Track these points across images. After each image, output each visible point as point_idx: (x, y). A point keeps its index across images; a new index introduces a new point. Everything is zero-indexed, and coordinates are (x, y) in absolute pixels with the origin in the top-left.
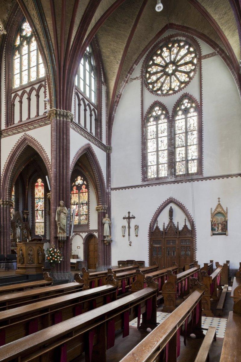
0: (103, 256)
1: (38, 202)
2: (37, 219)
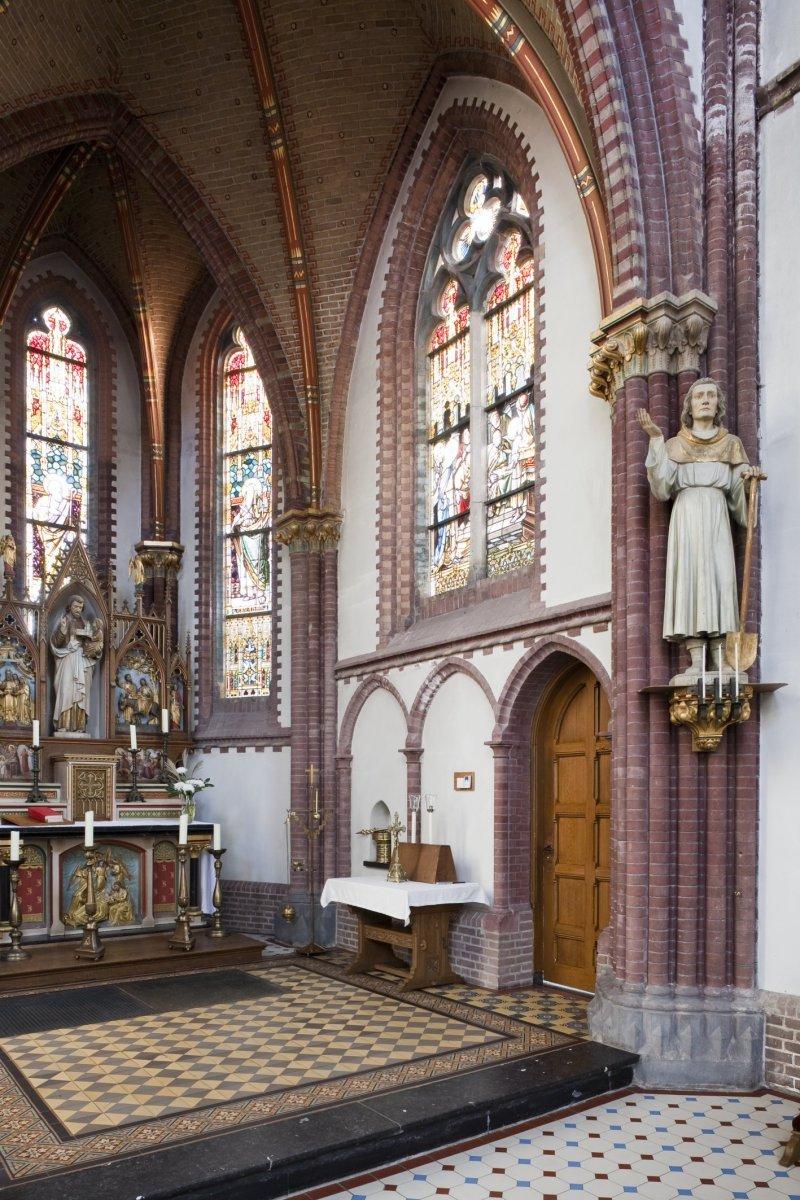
0: (657, 870)
1: (240, 479)
2: (236, 594)
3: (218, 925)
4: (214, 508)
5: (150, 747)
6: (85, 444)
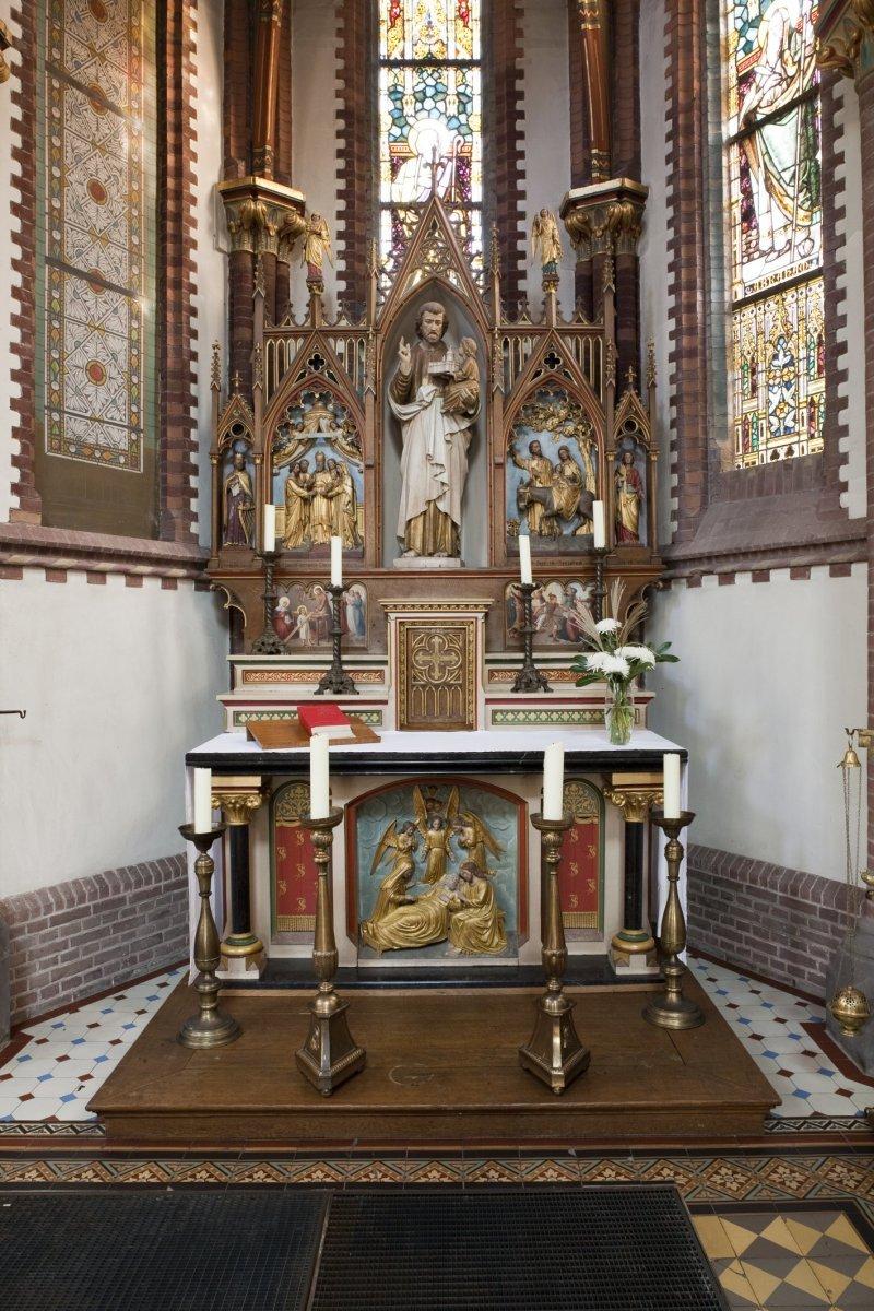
3: (673, 997)
4: (703, 91)
5: (574, 580)
6: (477, 56)
